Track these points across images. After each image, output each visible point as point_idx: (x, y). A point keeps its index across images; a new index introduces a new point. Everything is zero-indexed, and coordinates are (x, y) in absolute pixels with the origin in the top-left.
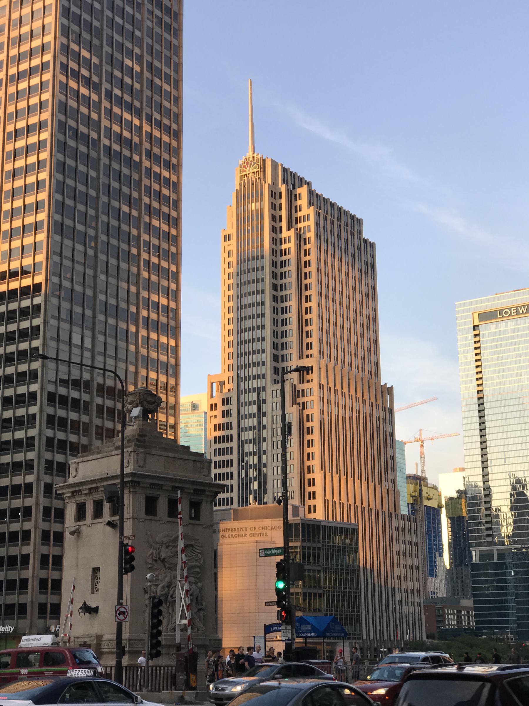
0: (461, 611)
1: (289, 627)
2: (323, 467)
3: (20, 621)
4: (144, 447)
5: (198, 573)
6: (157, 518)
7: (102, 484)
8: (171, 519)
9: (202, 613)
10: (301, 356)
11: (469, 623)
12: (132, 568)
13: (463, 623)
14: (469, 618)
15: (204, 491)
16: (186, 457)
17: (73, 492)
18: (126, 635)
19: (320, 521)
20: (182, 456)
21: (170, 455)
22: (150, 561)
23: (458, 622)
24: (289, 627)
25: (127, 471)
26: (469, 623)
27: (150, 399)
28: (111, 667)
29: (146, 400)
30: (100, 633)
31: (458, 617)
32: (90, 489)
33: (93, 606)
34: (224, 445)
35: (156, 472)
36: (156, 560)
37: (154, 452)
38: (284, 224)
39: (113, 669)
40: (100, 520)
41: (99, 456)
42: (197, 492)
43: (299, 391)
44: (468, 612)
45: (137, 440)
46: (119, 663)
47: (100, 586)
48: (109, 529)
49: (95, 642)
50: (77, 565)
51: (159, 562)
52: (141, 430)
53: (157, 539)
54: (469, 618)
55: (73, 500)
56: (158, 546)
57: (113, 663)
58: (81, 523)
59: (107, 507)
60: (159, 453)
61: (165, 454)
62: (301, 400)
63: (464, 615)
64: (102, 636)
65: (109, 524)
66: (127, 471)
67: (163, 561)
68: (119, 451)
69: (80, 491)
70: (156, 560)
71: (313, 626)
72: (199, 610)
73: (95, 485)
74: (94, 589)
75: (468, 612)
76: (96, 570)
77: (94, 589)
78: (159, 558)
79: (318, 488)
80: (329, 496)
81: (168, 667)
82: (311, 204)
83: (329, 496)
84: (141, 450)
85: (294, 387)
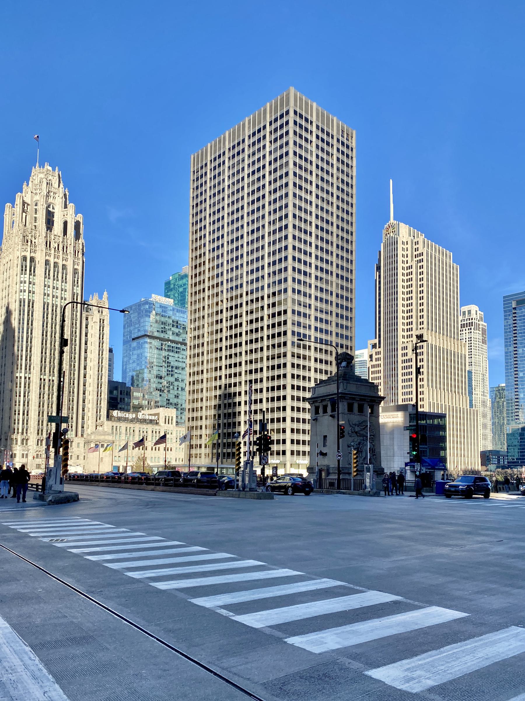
0: (500, 457)
1: (419, 464)
2: (428, 386)
3: (228, 459)
4: (346, 380)
5: (373, 438)
6: (373, 415)
7: (329, 397)
8: (359, 414)
9: (375, 456)
11: (504, 463)
12: (343, 436)
13: (501, 463)
14: (504, 460)
15: (375, 400)
16: (366, 384)
17: (313, 401)
18: (341, 466)
19: (427, 412)
20: (365, 384)
21: (359, 383)
22: (350, 433)
23: (498, 462)
24: (419, 464)
25: (340, 391)
26: (504, 463)
27: (348, 357)
28: (335, 479)
29: (347, 358)
30: (328, 464)
31: (498, 460)
32: (322, 400)
33: (325, 452)
35: (352, 392)
36: (353, 432)
37: (351, 382)
39: (336, 480)
40: (327, 414)
41: (325, 385)
42: (361, 400)
44: (504, 457)
45: (343, 377)
46: (339, 477)
47: (327, 444)
48: (330, 418)
49: (326, 468)
50: (316, 434)
51: (354, 433)
52: (345, 372)
53: (354, 423)
54: (504, 460)
55: (314, 405)
56: (354, 426)
57: (336, 477)
58: (317, 415)
59: (329, 409)
60: (354, 383)
61: (356, 383)
63: (501, 459)
64: (329, 466)
65: (331, 416)
66: (340, 391)
67: (356, 433)
68: (337, 382)
69: (317, 401)
70: (353, 432)
71: (429, 464)
72: (374, 455)
73: (324, 398)
74: (324, 445)
75: (504, 457)
76: (325, 437)
77: (324, 445)
78: (355, 431)
79: (426, 396)
80: (431, 400)
81: (360, 480)
83: (431, 400)
84: (345, 381)
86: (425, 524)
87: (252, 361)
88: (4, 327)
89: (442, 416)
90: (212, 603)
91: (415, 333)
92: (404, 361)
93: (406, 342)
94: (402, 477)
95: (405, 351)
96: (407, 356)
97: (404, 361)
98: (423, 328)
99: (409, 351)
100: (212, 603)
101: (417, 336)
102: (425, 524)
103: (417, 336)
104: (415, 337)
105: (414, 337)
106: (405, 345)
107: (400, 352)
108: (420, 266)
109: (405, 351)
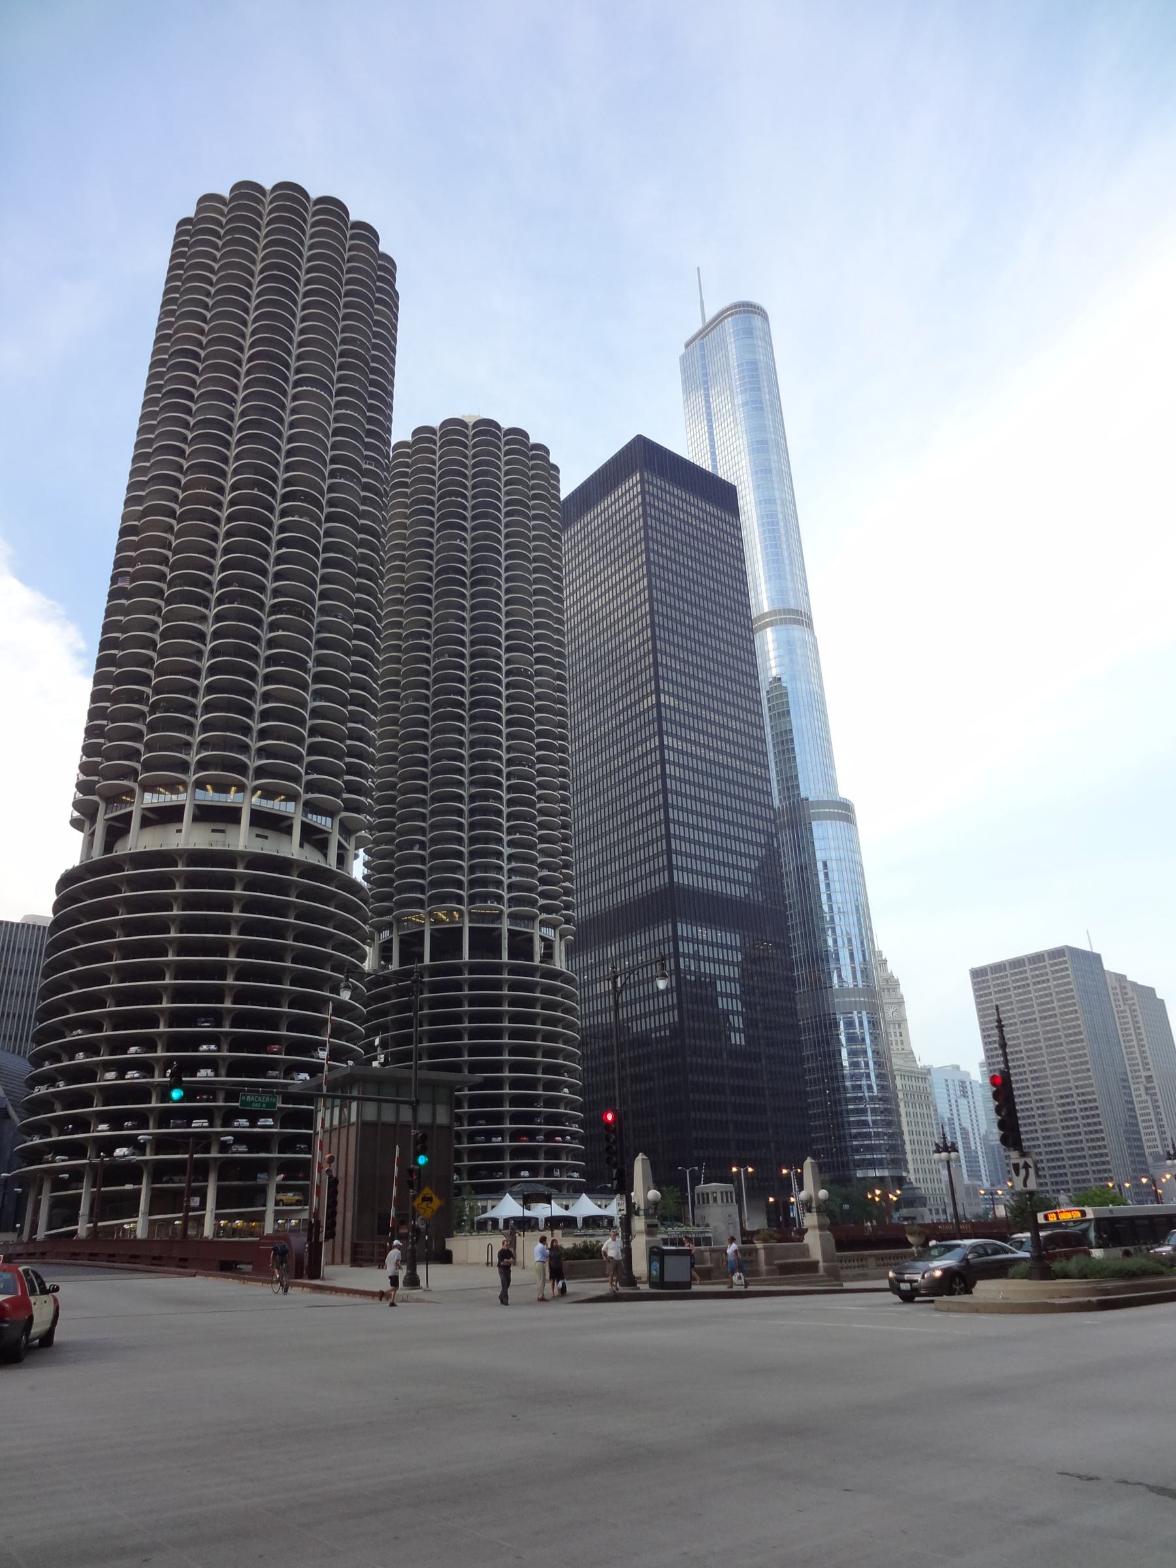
38: (1121, 1003)
62: (1149, 1092)
82: (1125, 1004)
91: (1144, 1074)
99: (1142, 1091)
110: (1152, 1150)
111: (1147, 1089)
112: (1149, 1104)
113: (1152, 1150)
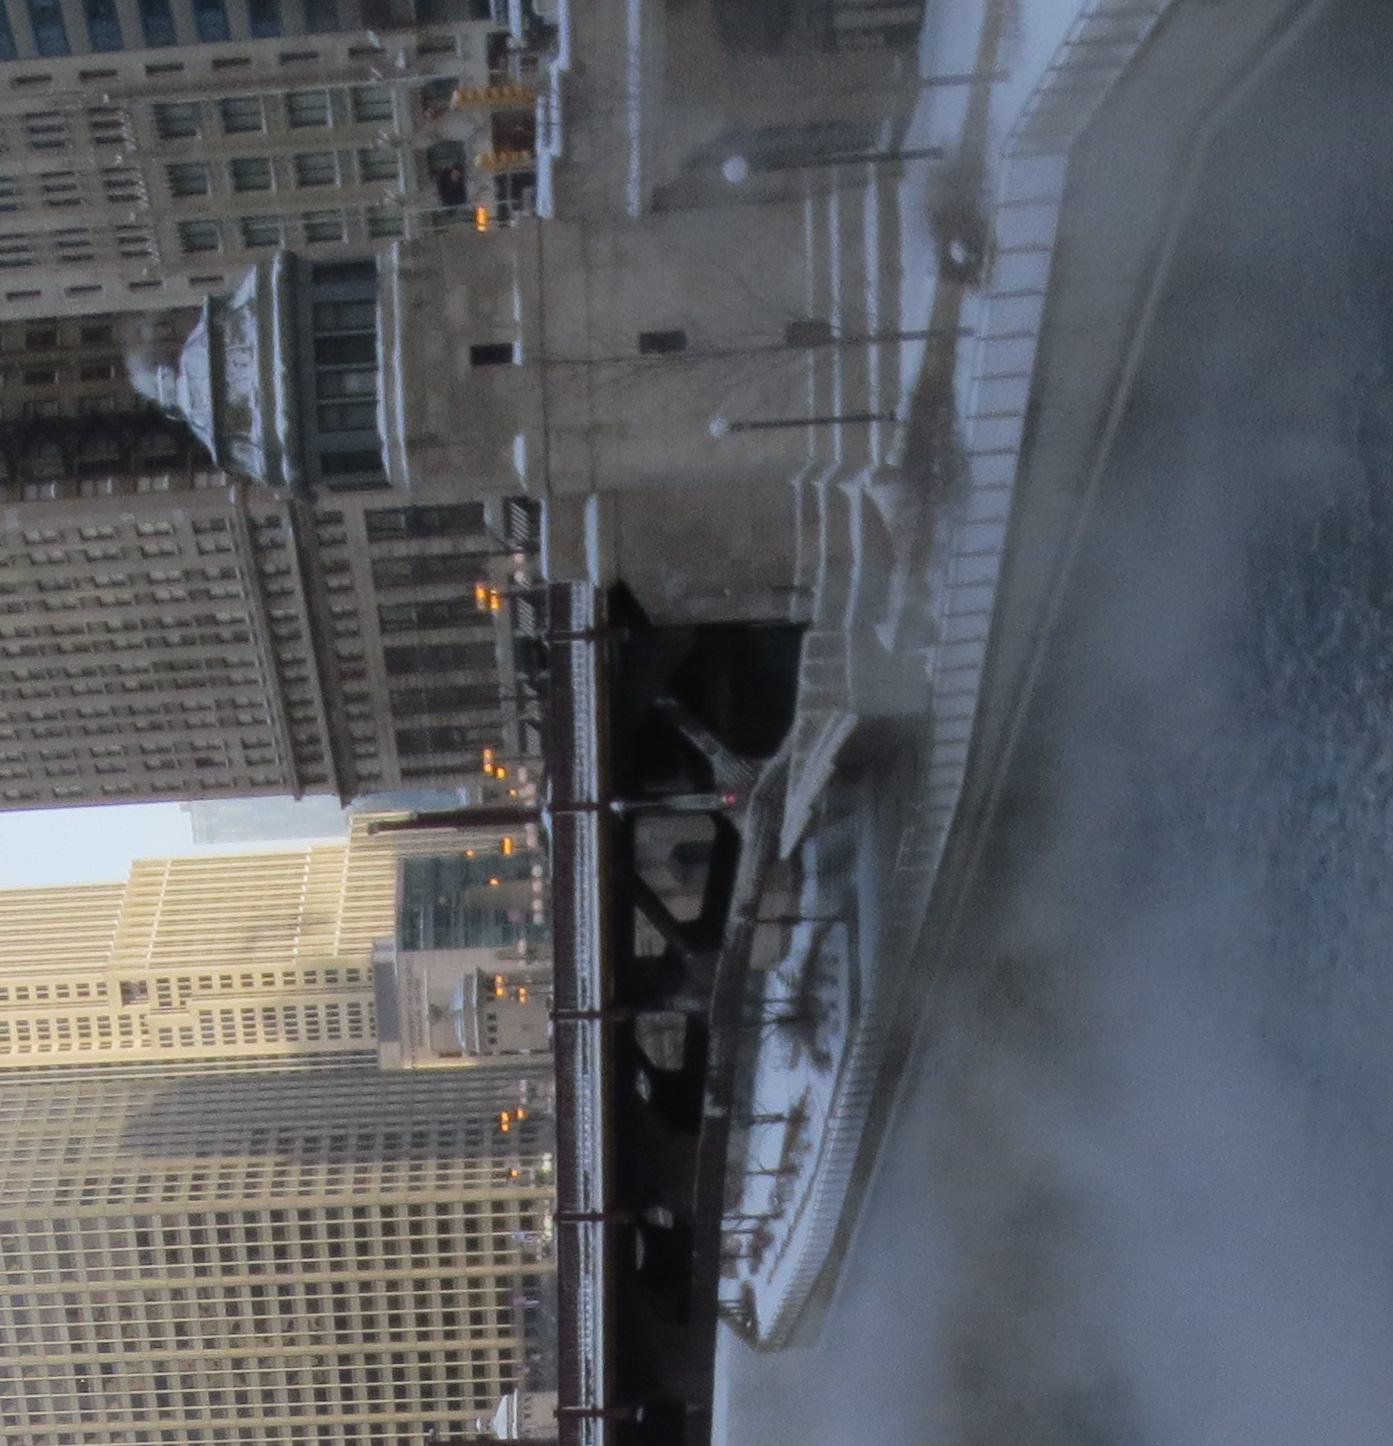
10: (103, 1003)
34: (323, 1026)
43: (162, 1004)
85: (154, 1012)
86: (568, 1010)
87: (321, 1406)
88: (723, 1152)
89: (489, 35)
90: (849, 638)
91: (114, 1008)
92: (209, 1038)
93: (145, 1037)
94: (520, 629)
95: (176, 1034)
96: (189, 1029)
97: (209, 1038)
98: (100, 985)
99: (174, 1020)
100: (849, 638)
101: (126, 1001)
102: (568, 1010)
103: (126, 1001)
104: (128, 1007)
105: (129, 1009)
106: (155, 1036)
107: (178, 1052)
108: (203, 987)
109: (176, 1034)
110: (366, 1026)
111: (165, 1004)
112: (215, 1006)
113: (366, 1026)
